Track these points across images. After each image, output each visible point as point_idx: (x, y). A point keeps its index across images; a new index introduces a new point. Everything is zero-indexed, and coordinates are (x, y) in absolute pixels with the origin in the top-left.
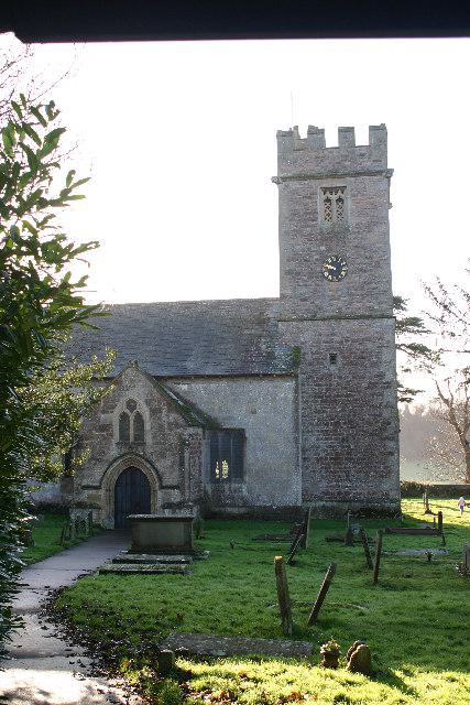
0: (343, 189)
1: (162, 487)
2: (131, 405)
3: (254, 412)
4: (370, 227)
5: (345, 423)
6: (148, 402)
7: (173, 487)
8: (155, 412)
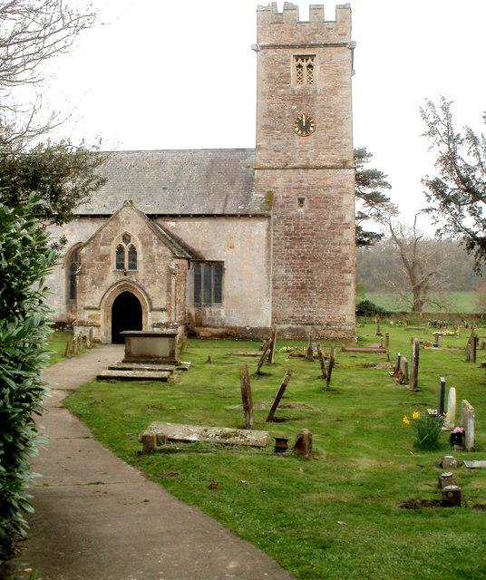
0: (313, 57)
1: (152, 310)
2: (126, 238)
3: (232, 247)
4: (334, 91)
7: (162, 310)
8: (145, 244)
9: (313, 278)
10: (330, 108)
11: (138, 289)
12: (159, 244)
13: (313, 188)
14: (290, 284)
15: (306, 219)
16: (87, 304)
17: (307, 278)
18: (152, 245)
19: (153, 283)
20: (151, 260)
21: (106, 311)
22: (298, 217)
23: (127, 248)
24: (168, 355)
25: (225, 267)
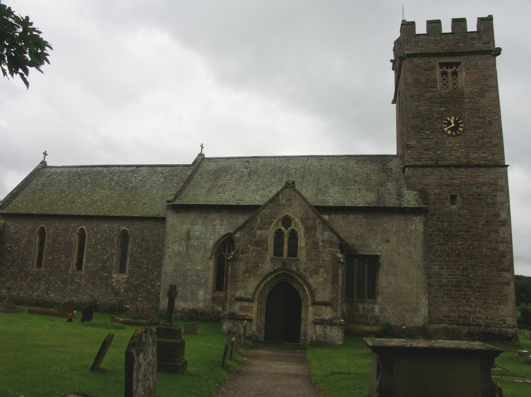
0: (457, 64)
1: (314, 304)
2: (287, 221)
3: (387, 241)
5: (465, 255)
6: (303, 221)
7: (326, 304)
8: (308, 229)
11: (297, 278)
12: (323, 230)
13: (465, 185)
14: (445, 281)
15: (460, 215)
16: (239, 294)
18: (315, 229)
19: (316, 272)
21: (260, 303)
25: (380, 261)
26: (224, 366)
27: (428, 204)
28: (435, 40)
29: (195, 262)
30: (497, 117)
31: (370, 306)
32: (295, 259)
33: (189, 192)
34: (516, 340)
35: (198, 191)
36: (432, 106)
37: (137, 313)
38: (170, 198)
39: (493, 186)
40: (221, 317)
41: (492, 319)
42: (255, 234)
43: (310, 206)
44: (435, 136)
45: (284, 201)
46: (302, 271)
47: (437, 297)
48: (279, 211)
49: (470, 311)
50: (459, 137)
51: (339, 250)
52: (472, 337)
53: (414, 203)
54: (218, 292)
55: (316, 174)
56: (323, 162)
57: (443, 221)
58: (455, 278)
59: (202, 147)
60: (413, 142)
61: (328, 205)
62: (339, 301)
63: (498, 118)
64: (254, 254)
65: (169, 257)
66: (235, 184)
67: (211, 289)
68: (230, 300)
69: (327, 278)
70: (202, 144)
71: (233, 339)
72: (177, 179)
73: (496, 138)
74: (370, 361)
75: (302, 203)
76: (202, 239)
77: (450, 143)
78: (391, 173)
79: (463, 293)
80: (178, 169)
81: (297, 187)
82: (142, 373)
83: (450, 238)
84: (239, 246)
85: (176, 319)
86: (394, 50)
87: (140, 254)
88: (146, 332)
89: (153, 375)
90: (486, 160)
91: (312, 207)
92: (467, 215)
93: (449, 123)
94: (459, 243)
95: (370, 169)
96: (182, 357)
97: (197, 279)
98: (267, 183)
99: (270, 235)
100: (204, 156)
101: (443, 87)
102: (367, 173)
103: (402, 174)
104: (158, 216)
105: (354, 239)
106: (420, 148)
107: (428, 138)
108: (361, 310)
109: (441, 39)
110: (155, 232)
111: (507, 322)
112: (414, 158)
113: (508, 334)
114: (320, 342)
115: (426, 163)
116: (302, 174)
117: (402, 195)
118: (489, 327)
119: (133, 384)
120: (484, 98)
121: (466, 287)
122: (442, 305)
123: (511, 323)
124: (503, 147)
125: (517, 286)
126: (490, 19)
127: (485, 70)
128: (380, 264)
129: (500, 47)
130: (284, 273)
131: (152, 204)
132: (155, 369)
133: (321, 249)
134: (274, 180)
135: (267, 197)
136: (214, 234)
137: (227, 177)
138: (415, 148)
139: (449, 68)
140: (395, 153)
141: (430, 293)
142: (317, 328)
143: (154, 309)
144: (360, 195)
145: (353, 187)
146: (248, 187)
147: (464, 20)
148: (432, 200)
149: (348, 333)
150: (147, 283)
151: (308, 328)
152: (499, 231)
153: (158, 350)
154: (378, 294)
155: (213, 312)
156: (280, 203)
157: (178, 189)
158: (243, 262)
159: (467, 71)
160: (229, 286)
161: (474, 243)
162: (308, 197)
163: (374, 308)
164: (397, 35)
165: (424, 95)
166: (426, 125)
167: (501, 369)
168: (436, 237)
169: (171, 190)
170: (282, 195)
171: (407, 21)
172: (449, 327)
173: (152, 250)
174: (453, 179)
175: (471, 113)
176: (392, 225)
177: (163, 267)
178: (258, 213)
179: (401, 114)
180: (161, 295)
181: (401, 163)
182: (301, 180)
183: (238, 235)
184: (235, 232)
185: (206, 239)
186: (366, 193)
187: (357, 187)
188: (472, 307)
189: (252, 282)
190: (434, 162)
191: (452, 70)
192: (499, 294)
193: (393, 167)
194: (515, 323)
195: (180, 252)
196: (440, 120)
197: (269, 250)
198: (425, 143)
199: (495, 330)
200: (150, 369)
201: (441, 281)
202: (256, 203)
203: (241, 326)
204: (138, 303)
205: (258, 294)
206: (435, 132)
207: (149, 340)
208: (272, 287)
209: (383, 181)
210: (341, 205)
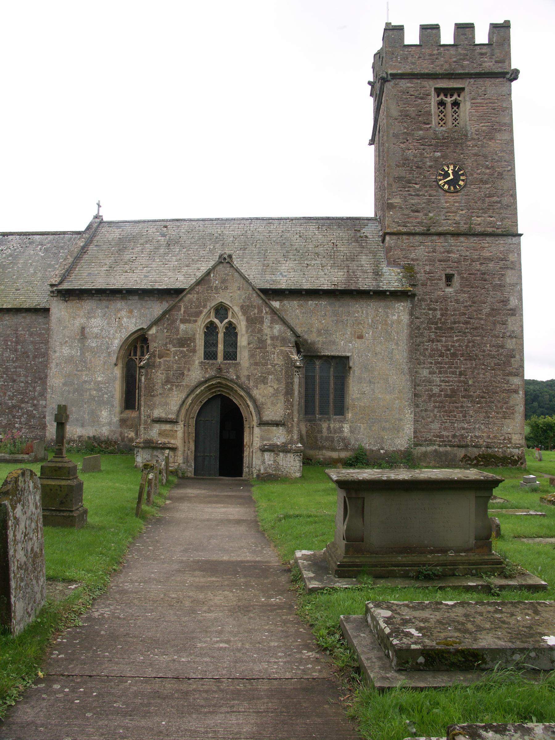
0: (460, 91)
1: (262, 424)
3: (360, 337)
4: (490, 135)
5: (462, 355)
6: (245, 309)
7: (277, 424)
8: (252, 321)
9: (466, 383)
10: (485, 157)
11: (238, 389)
14: (436, 390)
15: (457, 301)
16: (157, 413)
17: (460, 382)
18: (262, 322)
19: (264, 381)
20: (261, 344)
22: (445, 298)
23: (221, 326)
24: (472, 542)
25: (351, 364)
26: (139, 513)
27: (415, 285)
28: (431, 55)
29: (94, 371)
30: (509, 168)
31: (337, 425)
32: (233, 364)
33: (81, 272)
34: (522, 463)
35: (95, 269)
36: (424, 149)
37: (15, 446)
38: (54, 281)
39: (502, 262)
40: (133, 446)
41: (495, 437)
42: (178, 330)
43: (254, 290)
44: (427, 191)
45: (217, 282)
46: (243, 379)
47: (426, 410)
48: (210, 297)
49: (467, 429)
50: (459, 194)
51: (294, 350)
52: (469, 462)
53: (397, 284)
54: (128, 412)
55: (262, 244)
56: (272, 227)
57: (435, 310)
58: (449, 386)
59: (99, 206)
60: (396, 200)
61: (279, 287)
62: (296, 420)
63: (511, 169)
64: (176, 358)
65: (57, 364)
66: (148, 258)
67: (118, 407)
68: (146, 422)
69: (278, 388)
70: (99, 201)
71: (151, 476)
72: (63, 253)
73: (508, 196)
74: (336, 497)
75: (243, 285)
76: (103, 337)
77: (446, 202)
78: (367, 243)
79: (460, 405)
80: (64, 237)
81: (235, 263)
82: (21, 531)
83: (443, 331)
84: (155, 347)
85: (70, 450)
86: (373, 67)
87: (14, 362)
88: (23, 474)
89: (38, 533)
90: (493, 227)
91: (257, 291)
92: (466, 301)
93: (447, 175)
94: (455, 339)
95: (337, 237)
96: (80, 504)
97: (98, 395)
98: (193, 257)
99: (198, 330)
100: (102, 219)
101: (439, 123)
102: (333, 243)
103: (381, 244)
104: (38, 307)
105: (315, 334)
106: (407, 208)
107: (418, 195)
108: (325, 430)
109: (439, 54)
110: (35, 330)
111: (513, 441)
112: (398, 223)
113: (513, 456)
114: (270, 475)
115: (414, 229)
116: (243, 244)
117: (380, 273)
118: (490, 448)
119: (9, 547)
120: (493, 141)
121: (463, 397)
122: (432, 422)
123: (517, 442)
124: (516, 209)
125: (526, 394)
126: (506, 26)
127: (496, 101)
128: (350, 368)
129: (518, 68)
130: (219, 383)
131: (28, 290)
132: (39, 525)
133: (269, 348)
134: (203, 252)
135: (193, 276)
136: (120, 331)
137: (137, 250)
138: (399, 208)
139: (449, 96)
140: (371, 214)
141: (417, 406)
142: (266, 456)
143: (38, 439)
144: (323, 273)
145: (313, 262)
146: (167, 263)
147: (471, 26)
148: (422, 280)
149: (307, 461)
150: (27, 402)
151: (254, 456)
152: (507, 323)
153: (44, 498)
154: (348, 409)
155: (123, 440)
156: (212, 285)
157: (66, 267)
158: (162, 369)
159: (473, 101)
160: (142, 403)
161: (475, 338)
162: (251, 276)
163: (343, 427)
164: (378, 45)
165: (413, 134)
166: (415, 176)
167: (502, 501)
168: (426, 331)
169: (55, 269)
170: (214, 273)
171: (393, 24)
172: (441, 449)
173: (31, 356)
174: (448, 252)
175: (476, 161)
176: (367, 314)
177: (48, 379)
178: (181, 300)
179: (381, 161)
180: (47, 418)
181: (380, 229)
182: (242, 252)
183: (153, 331)
184: (150, 327)
185: (109, 338)
186: (332, 271)
187: (319, 262)
188: (470, 422)
189: (175, 396)
190: (425, 229)
191: (452, 99)
192: (505, 406)
193: (368, 234)
194: (523, 442)
195: (72, 357)
196: (434, 169)
197: (198, 352)
198: (413, 201)
199: (498, 451)
200: (33, 525)
201: (431, 390)
202: (178, 285)
203: (161, 458)
204: (15, 431)
205: (183, 411)
206: (426, 187)
207: (28, 485)
208: (203, 402)
209: (356, 254)
210: (297, 288)
